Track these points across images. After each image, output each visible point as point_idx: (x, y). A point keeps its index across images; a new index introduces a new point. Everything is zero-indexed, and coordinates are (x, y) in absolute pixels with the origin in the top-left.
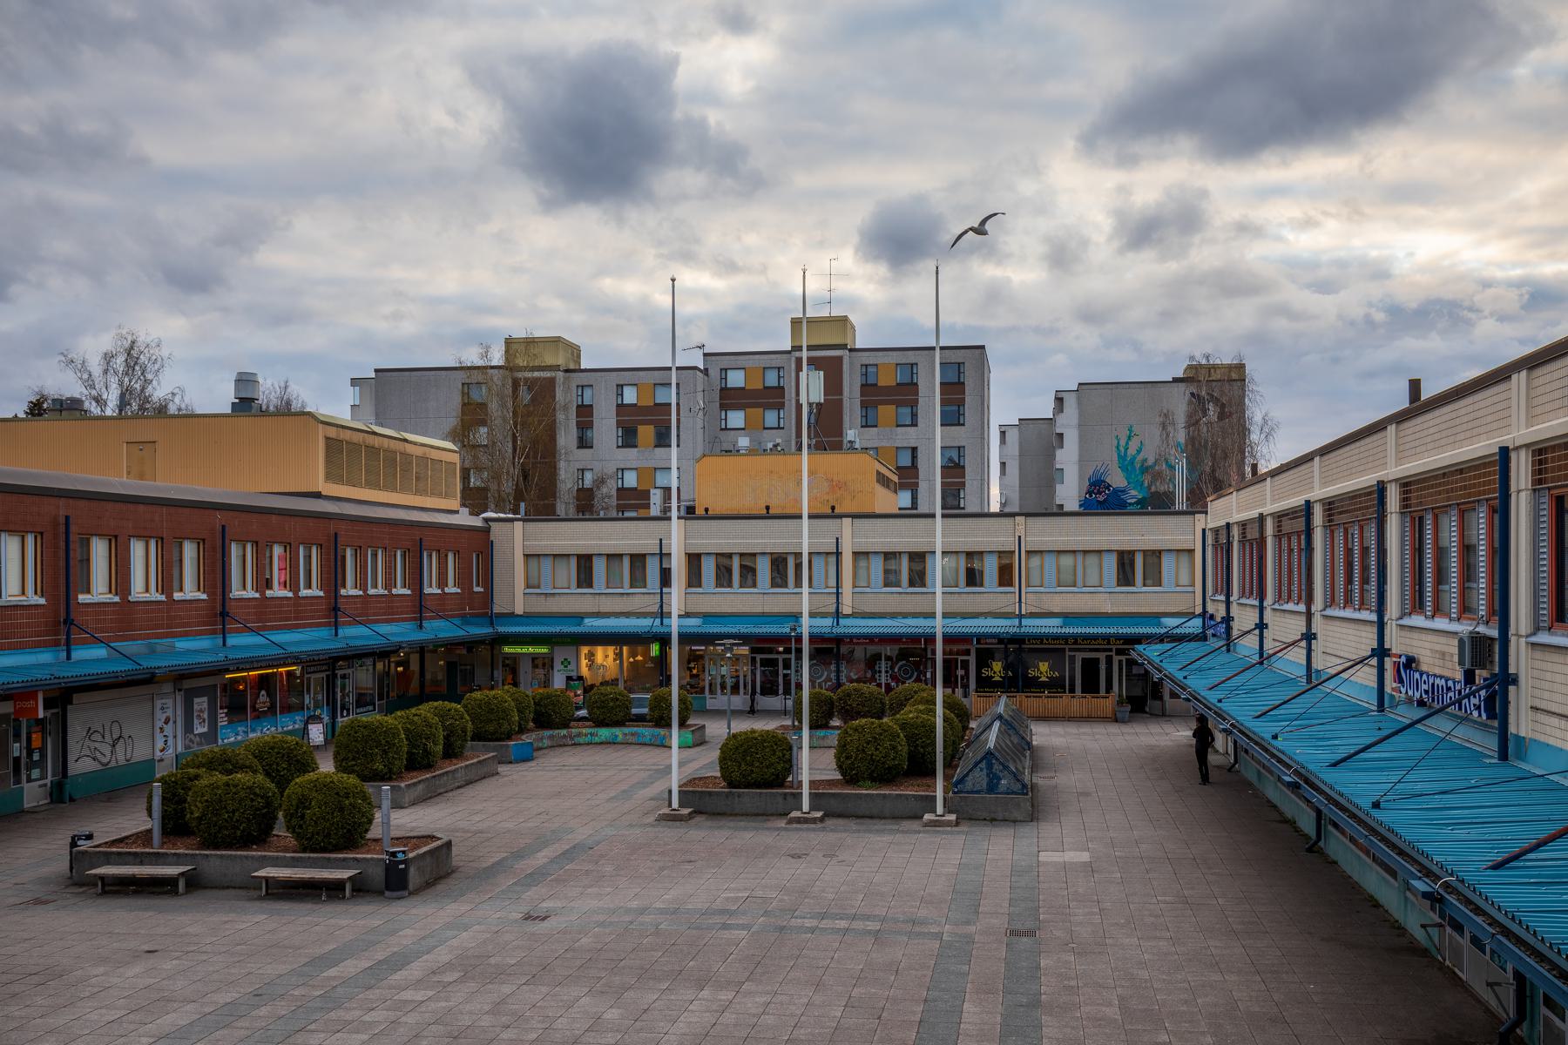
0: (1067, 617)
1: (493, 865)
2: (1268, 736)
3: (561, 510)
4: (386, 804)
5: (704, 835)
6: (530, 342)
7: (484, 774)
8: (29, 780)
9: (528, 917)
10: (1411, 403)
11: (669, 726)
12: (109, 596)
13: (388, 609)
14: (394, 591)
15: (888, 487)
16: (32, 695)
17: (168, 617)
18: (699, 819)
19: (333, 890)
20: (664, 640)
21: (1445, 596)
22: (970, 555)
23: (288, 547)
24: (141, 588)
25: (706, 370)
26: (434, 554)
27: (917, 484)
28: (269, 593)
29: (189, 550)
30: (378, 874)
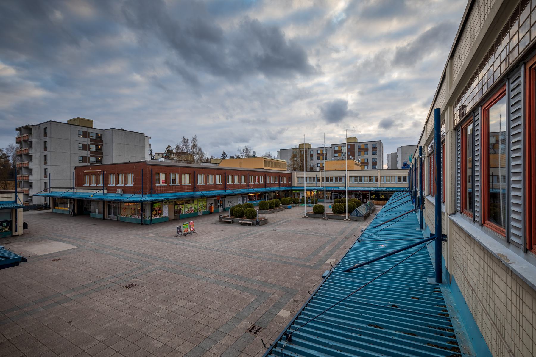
0: (387, 187)
1: (275, 222)
5: (309, 220)
7: (282, 210)
8: (220, 208)
9: (274, 230)
11: (304, 203)
13: (274, 185)
15: (358, 166)
16: (219, 197)
17: (240, 186)
18: (309, 218)
19: (249, 224)
20: (324, 190)
22: (370, 177)
27: (368, 165)
28: (255, 183)
29: (243, 177)
30: (255, 222)
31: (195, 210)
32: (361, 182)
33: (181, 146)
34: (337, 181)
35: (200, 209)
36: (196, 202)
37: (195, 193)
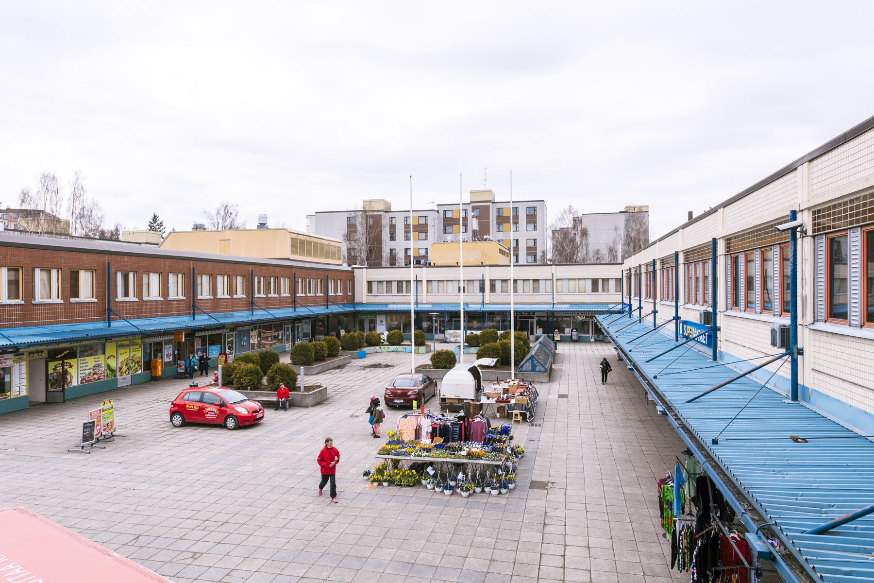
2: (628, 351)
3: (384, 264)
4: (302, 373)
6: (371, 201)
9: (352, 416)
10: (689, 220)
12: (210, 296)
13: (315, 301)
14: (317, 295)
15: (504, 255)
21: (698, 296)
23: (161, 275)
24: (222, 293)
25: (438, 211)
26: (333, 281)
28: (269, 295)
31: (109, 372)
32: (372, 293)
33: (33, 193)
34: (400, 290)
35: (124, 368)
36: (111, 349)
37: (109, 326)
